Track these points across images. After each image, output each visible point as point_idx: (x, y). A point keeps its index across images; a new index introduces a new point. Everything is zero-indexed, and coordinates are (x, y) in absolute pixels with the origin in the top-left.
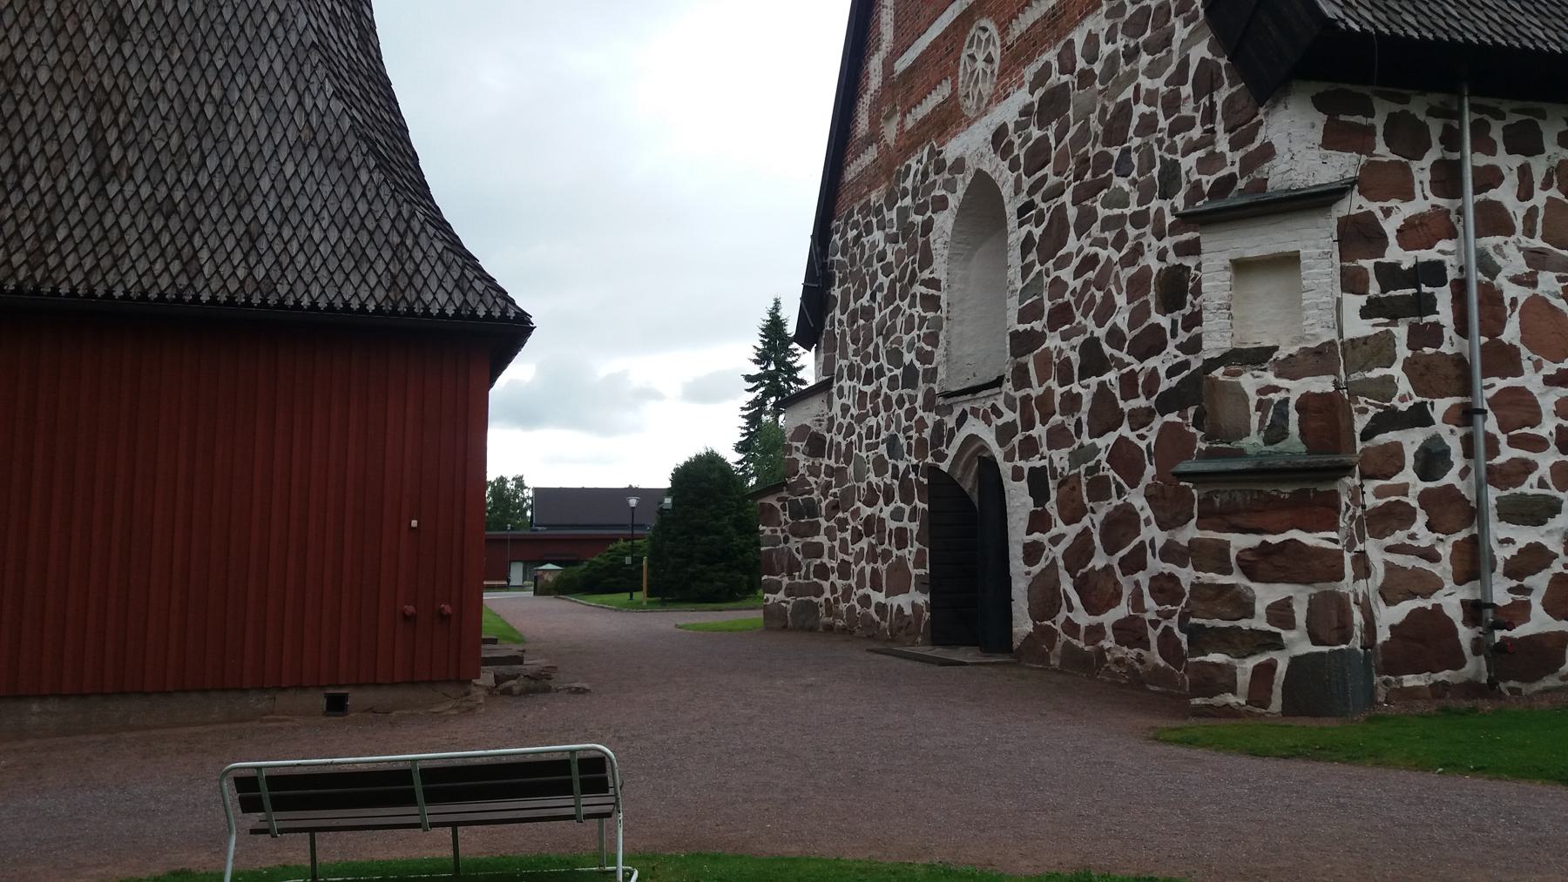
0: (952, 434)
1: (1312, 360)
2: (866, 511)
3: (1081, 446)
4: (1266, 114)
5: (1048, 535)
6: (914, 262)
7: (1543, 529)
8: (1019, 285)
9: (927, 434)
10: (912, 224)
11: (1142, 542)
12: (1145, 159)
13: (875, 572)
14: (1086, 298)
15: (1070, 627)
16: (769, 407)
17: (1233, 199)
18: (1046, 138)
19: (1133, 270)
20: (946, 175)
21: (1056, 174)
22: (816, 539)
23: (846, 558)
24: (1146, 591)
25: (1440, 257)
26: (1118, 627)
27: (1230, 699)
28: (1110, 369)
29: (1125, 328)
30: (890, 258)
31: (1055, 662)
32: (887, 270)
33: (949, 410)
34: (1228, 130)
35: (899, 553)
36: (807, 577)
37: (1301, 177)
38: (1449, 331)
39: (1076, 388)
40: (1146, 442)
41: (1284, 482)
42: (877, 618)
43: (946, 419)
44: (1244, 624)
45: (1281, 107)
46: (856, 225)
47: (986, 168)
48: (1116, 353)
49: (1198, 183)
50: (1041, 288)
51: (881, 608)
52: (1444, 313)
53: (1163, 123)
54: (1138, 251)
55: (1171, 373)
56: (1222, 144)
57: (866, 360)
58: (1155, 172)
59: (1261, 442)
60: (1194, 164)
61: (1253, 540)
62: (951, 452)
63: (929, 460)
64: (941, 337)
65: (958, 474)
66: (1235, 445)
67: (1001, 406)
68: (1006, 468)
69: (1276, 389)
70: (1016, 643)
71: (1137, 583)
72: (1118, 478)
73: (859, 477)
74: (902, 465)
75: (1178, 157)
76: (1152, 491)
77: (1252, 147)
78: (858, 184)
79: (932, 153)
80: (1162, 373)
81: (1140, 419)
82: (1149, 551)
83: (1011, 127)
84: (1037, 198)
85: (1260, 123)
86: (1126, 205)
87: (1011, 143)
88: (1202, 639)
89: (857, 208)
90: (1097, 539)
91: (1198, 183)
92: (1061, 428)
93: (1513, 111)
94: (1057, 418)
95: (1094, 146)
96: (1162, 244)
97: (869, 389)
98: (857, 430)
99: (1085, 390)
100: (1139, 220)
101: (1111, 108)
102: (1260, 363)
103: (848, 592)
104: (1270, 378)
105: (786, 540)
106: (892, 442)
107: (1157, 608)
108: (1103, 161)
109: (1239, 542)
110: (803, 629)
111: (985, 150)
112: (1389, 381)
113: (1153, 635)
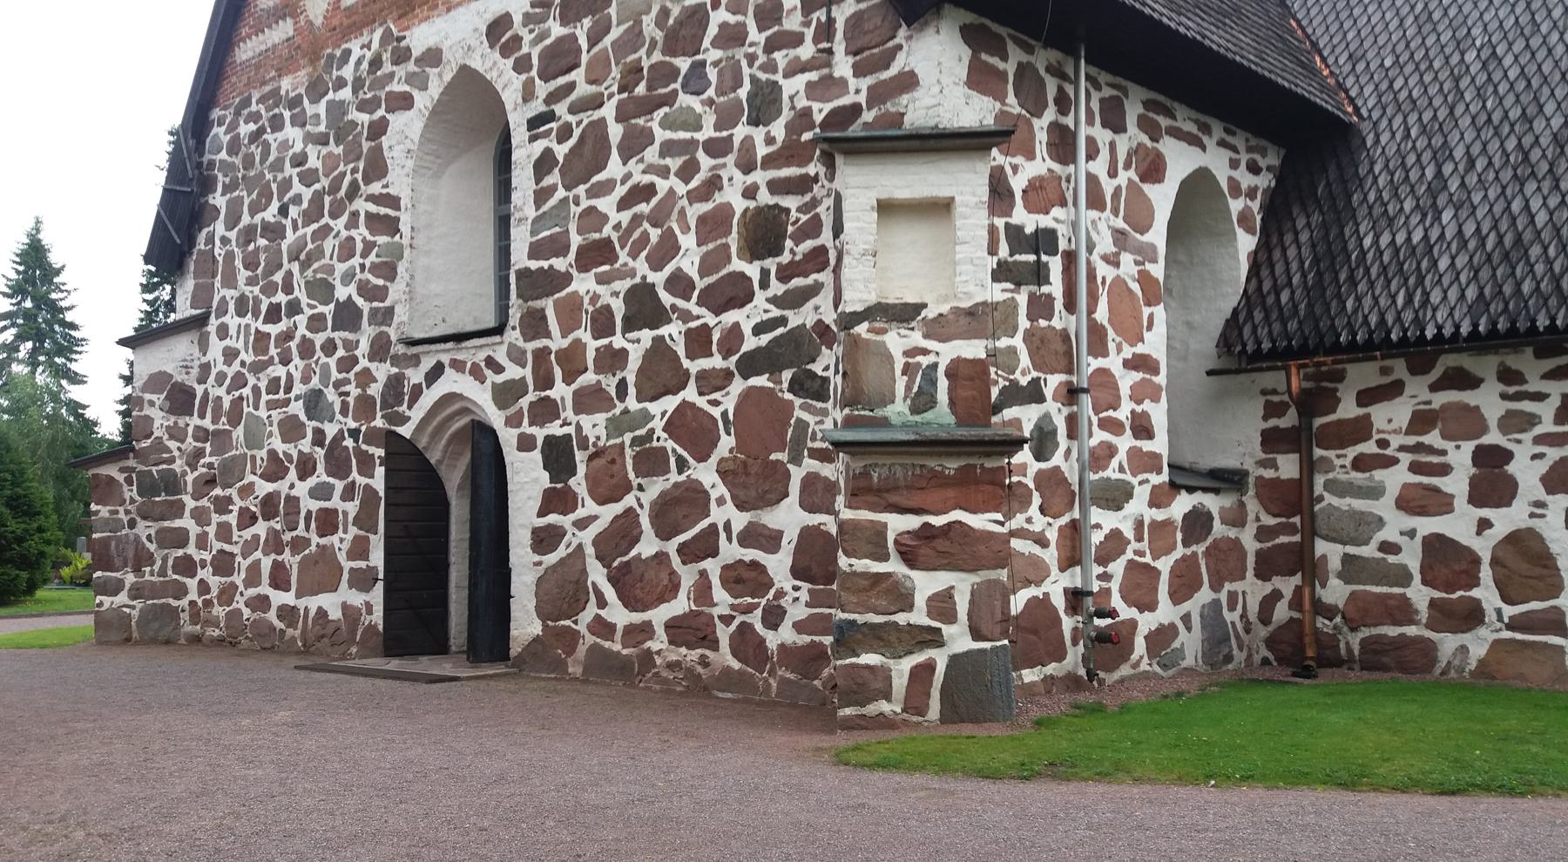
0: (417, 392)
1: (964, 321)
2: (264, 488)
3: (626, 412)
4: (909, 38)
5: (572, 517)
6: (355, 170)
7: (1121, 514)
8: (531, 213)
9: (375, 390)
10: (354, 124)
11: (713, 526)
12: (728, 75)
13: (278, 568)
14: (636, 235)
15: (603, 628)
16: (21, 355)
17: (854, 130)
18: (574, 38)
19: (707, 207)
20: (411, 67)
21: (591, 82)
22: (177, 523)
23: (227, 547)
24: (716, 581)
25: (1052, 225)
26: (672, 626)
27: (884, 707)
28: (669, 321)
29: (695, 277)
30: (313, 162)
31: (575, 669)
32: (308, 178)
33: (415, 361)
34: (852, 51)
35: (323, 541)
36: (163, 573)
37: (948, 115)
38: (1059, 305)
39: (618, 341)
40: (721, 409)
41: (949, 455)
42: (279, 625)
43: (408, 372)
44: (901, 618)
45: (931, 30)
46: (255, 117)
47: (476, 64)
48: (680, 303)
49: (807, 113)
50: (567, 218)
51: (287, 613)
52: (1055, 287)
53: (755, 35)
54: (714, 184)
55: (758, 330)
56: (843, 66)
57: (270, 289)
58: (743, 93)
59: (907, 412)
60: (802, 88)
61: (913, 522)
62: (417, 414)
63: (379, 422)
64: (401, 269)
65: (422, 443)
66: (879, 413)
67: (501, 356)
68: (508, 438)
69: (925, 352)
70: (515, 649)
71: (703, 574)
72: (680, 450)
73: (253, 441)
74: (331, 430)
75: (778, 77)
76: (730, 466)
77: (885, 75)
78: (258, 66)
79: (387, 37)
80: (747, 330)
81: (712, 382)
82: (723, 536)
83: (517, 19)
84: (561, 109)
85: (900, 47)
86: (699, 128)
87: (517, 39)
88: (849, 637)
89: (256, 96)
90: (645, 521)
91: (807, 113)
92: (598, 389)
93: (1108, 84)
94: (589, 378)
95: (649, 54)
96: (750, 179)
97: (274, 330)
98: (252, 381)
99: (637, 345)
100: (716, 148)
101: (676, 12)
102: (907, 320)
103: (228, 593)
104: (916, 338)
105: (132, 524)
106: (314, 403)
107: (731, 600)
108: (664, 73)
109: (898, 524)
110: (154, 641)
111: (474, 43)
112: (1012, 351)
113: (724, 634)
